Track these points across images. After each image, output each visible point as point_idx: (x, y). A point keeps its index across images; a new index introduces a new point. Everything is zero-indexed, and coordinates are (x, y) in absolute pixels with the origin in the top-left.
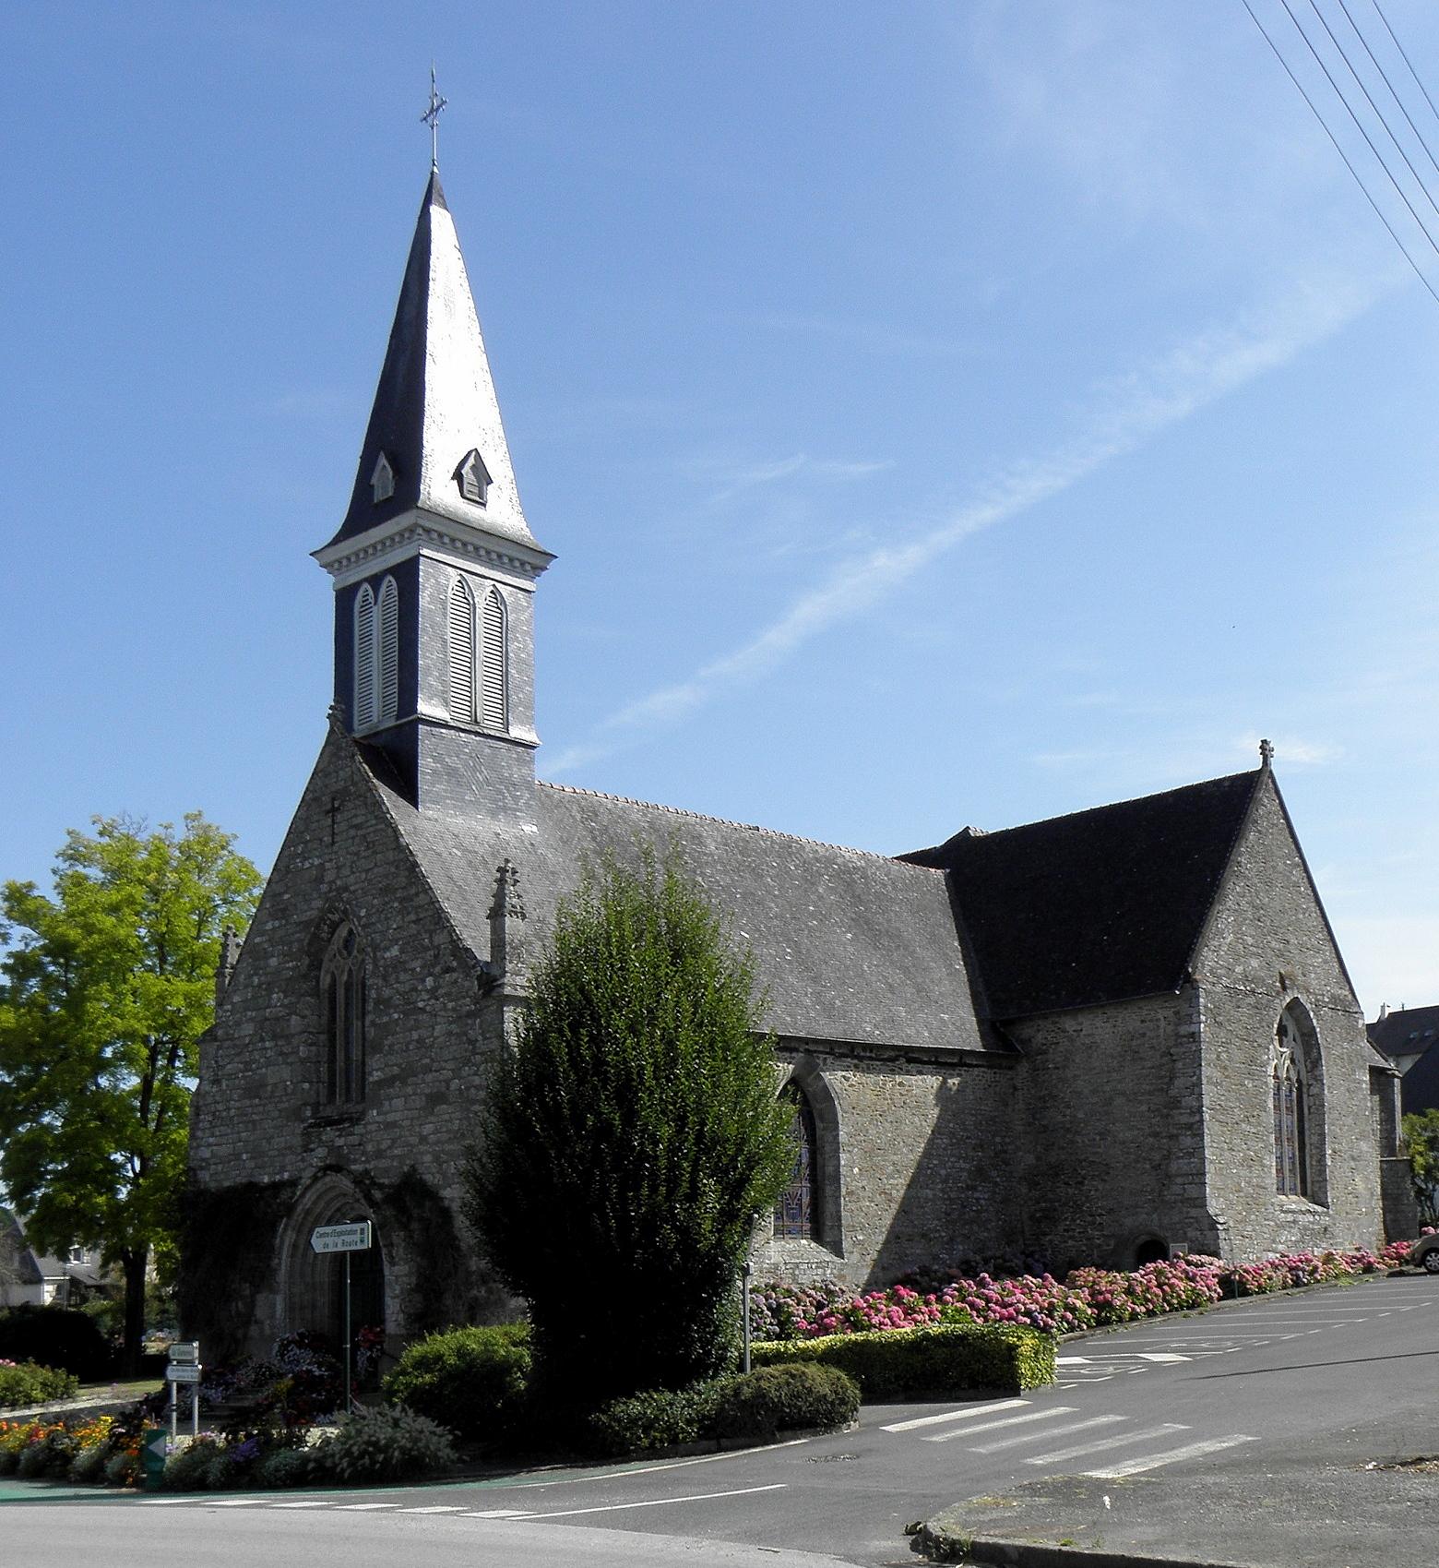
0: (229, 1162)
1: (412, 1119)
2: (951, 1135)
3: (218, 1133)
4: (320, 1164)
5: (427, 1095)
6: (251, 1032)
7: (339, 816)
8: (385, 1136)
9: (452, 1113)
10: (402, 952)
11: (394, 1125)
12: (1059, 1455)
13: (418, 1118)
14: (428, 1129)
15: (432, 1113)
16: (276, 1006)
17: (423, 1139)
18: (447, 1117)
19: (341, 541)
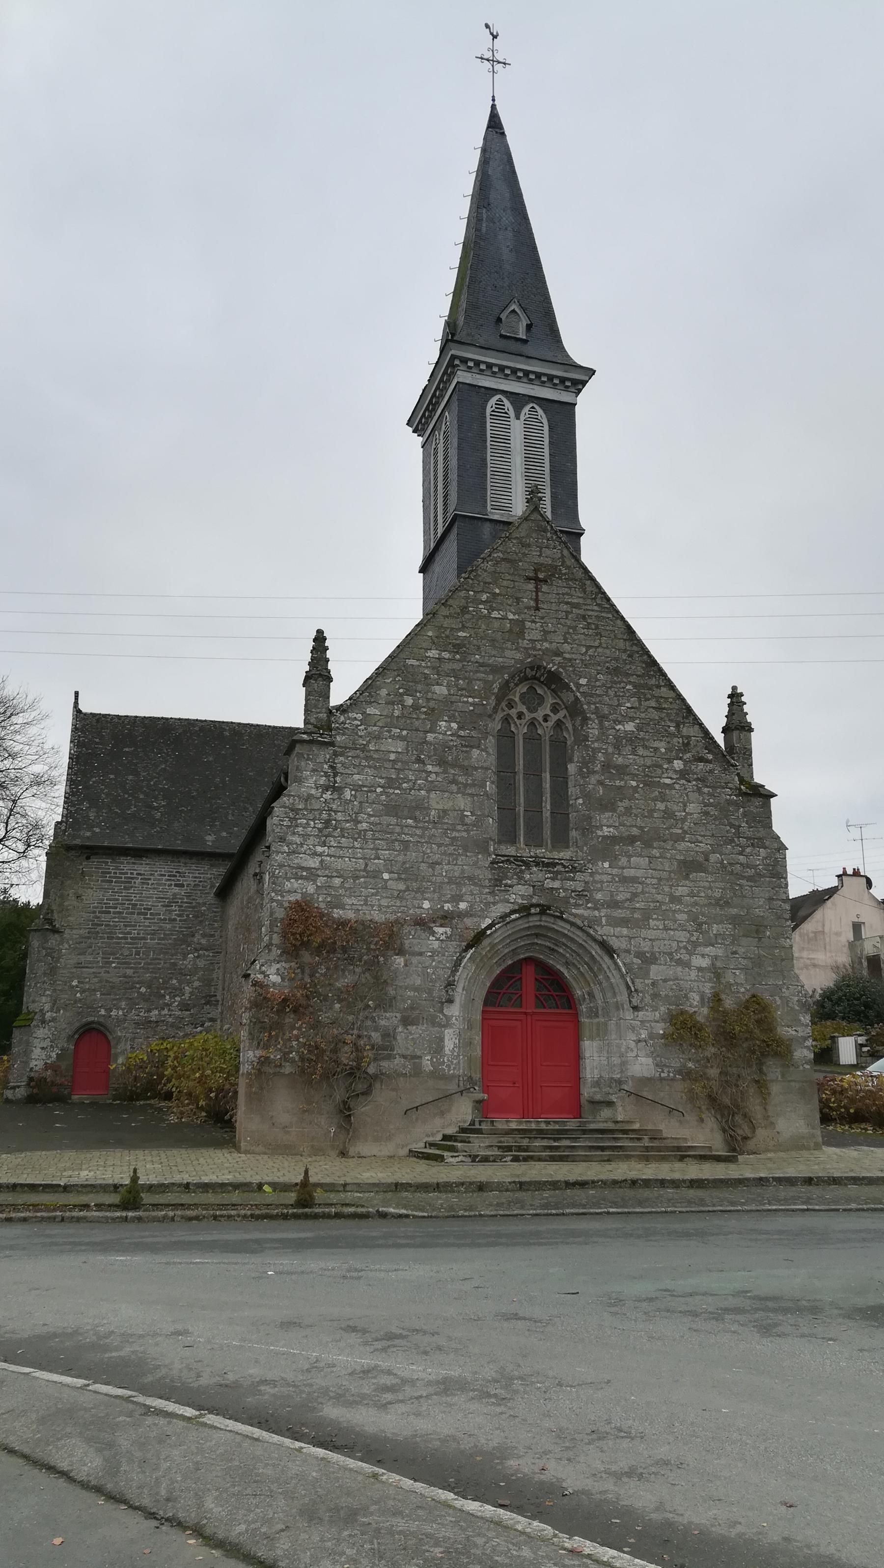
0: (358, 877)
1: (660, 879)
2: (142, 1070)
3: (359, 855)
4: (520, 901)
5: (679, 861)
6: (400, 750)
7: (774, 1088)
8: (621, 889)
9: (713, 881)
10: (639, 728)
11: (634, 880)
12: (610, 971)
13: (668, 880)
14: (681, 891)
15: (687, 877)
16: (445, 734)
17: (674, 899)
18: (707, 884)
19: (484, 162)
